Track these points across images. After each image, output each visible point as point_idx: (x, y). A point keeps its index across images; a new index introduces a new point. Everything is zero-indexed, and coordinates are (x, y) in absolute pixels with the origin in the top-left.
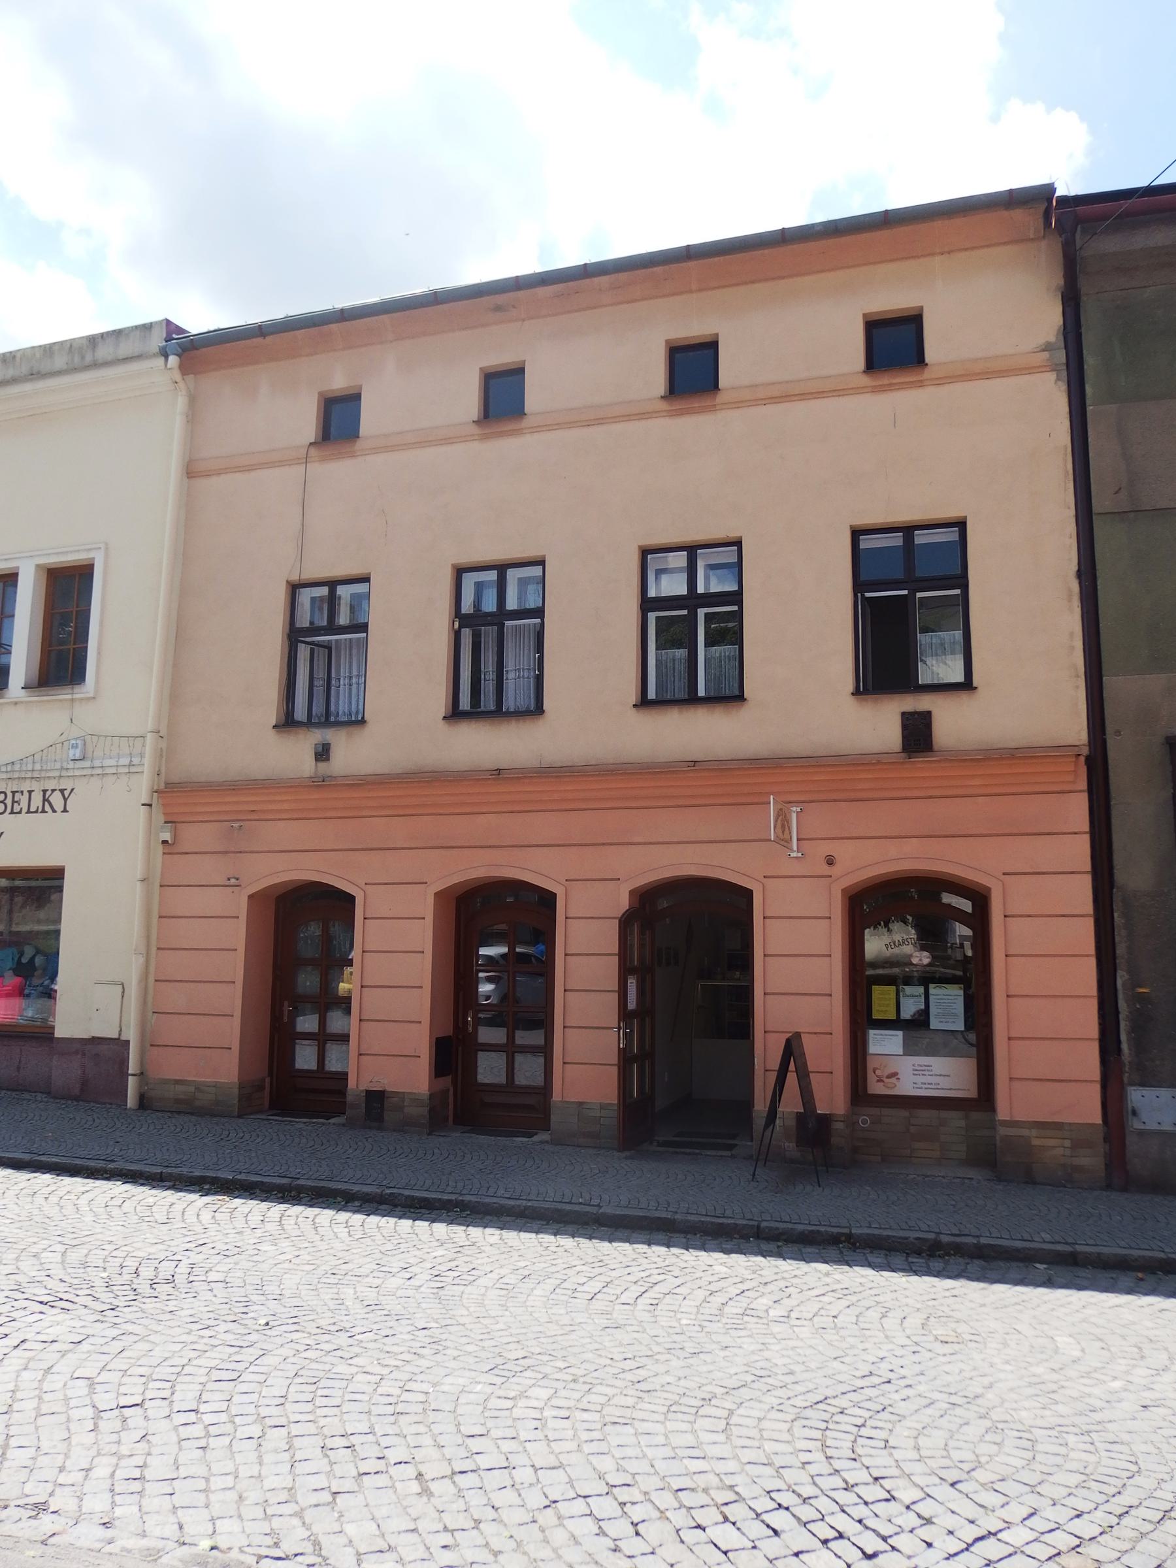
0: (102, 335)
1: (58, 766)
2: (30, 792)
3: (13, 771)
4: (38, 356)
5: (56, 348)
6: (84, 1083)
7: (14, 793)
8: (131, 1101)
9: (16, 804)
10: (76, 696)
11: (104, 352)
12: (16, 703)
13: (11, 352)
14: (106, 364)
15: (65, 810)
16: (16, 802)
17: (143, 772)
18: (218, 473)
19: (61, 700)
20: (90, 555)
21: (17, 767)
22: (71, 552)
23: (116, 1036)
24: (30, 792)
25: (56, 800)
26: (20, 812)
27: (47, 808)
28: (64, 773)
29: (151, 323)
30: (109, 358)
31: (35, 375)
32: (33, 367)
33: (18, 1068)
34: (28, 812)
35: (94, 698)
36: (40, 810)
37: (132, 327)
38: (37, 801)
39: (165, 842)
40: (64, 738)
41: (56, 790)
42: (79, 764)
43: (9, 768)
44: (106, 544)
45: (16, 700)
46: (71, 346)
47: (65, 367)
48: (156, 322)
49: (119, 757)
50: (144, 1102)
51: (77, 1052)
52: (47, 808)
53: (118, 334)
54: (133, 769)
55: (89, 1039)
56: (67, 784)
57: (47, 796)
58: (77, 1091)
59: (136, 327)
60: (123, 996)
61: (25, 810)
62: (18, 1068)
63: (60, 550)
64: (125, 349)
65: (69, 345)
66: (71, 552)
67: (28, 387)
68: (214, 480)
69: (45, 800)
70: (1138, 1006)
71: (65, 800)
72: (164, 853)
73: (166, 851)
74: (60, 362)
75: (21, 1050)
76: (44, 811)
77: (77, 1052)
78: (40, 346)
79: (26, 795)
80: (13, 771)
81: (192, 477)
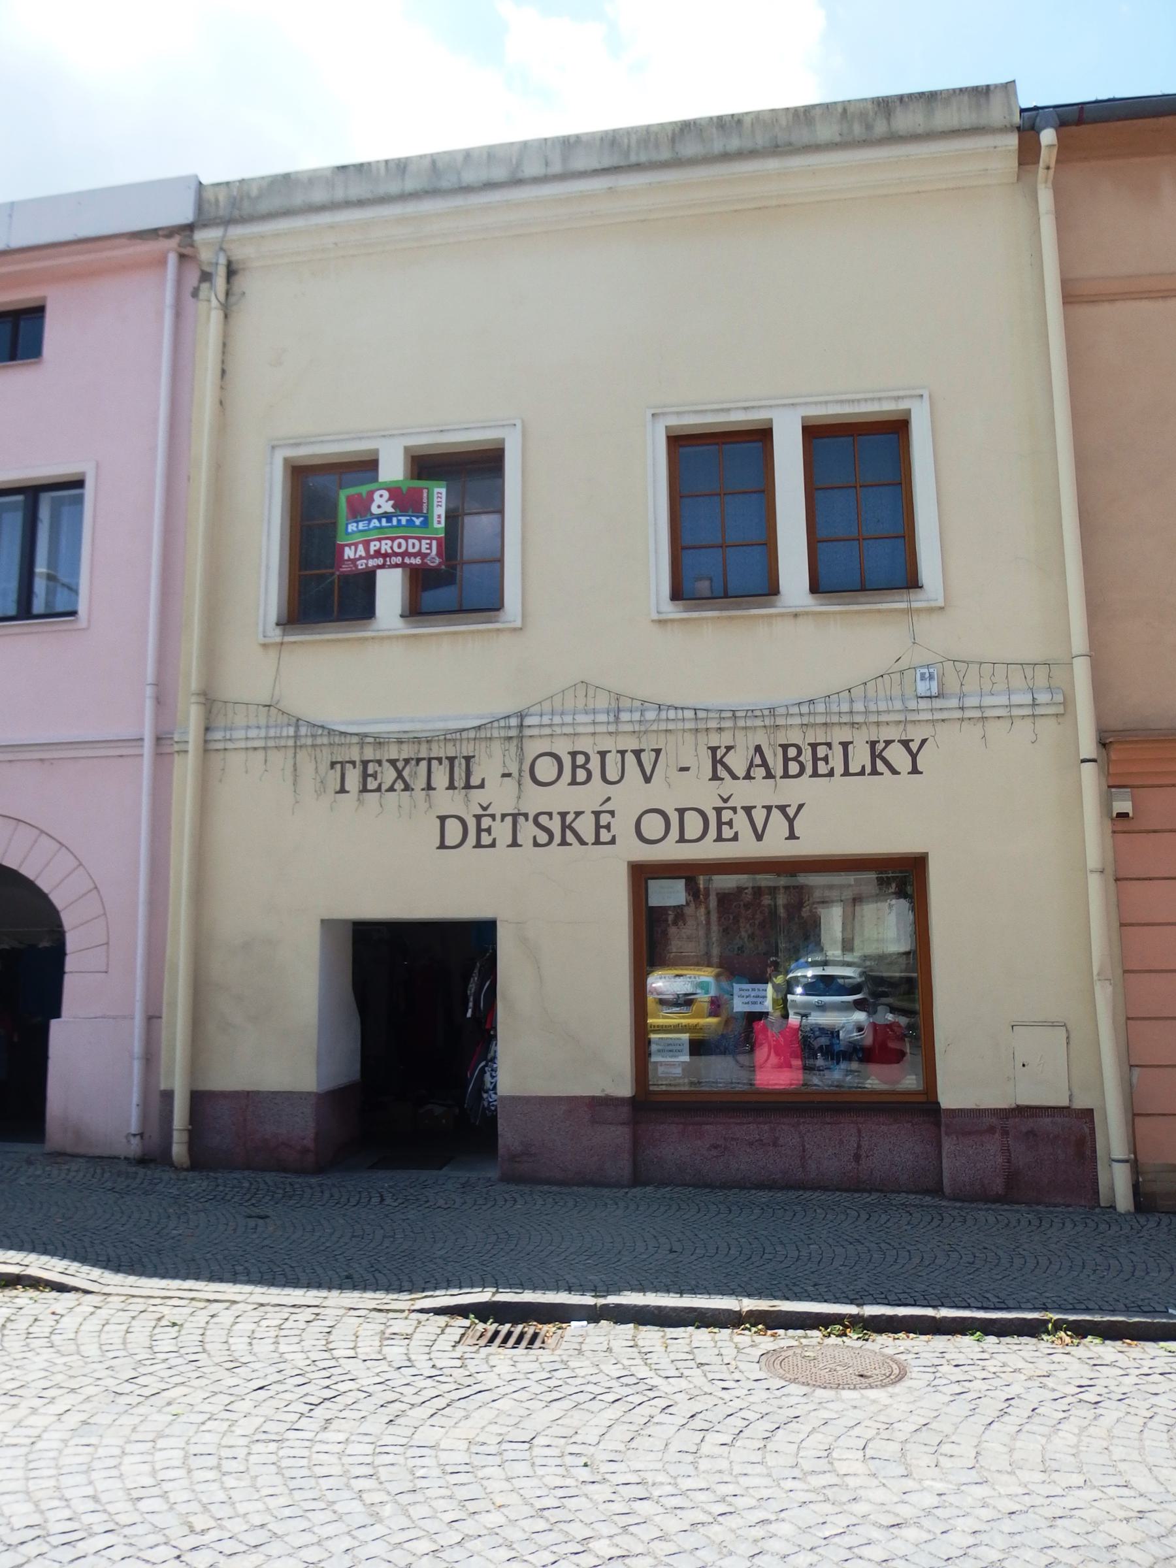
0: (901, 98)
1: (263, 733)
2: (845, 745)
3: (815, 714)
4: (784, 122)
5: (818, 111)
6: (1012, 1177)
7: (814, 746)
8: (1124, 1201)
9: (370, 779)
10: (915, 605)
11: (904, 121)
12: (796, 615)
13: (733, 115)
14: (693, 162)
15: (915, 770)
16: (371, 775)
17: (186, 752)
18: (1112, 298)
19: (879, 611)
20: (903, 405)
21: (820, 708)
22: (866, 400)
23: (1065, 1103)
24: (845, 745)
25: (897, 756)
26: (831, 774)
27: (880, 766)
28: (911, 717)
29: (988, 86)
30: (920, 130)
31: (777, 149)
32: (776, 137)
33: (857, 1158)
34: (846, 773)
35: (521, 629)
36: (868, 770)
37: (954, 90)
38: (860, 757)
39: (1123, 816)
40: (903, 665)
41: (894, 741)
42: (938, 704)
43: (805, 709)
44: (523, 421)
45: (798, 610)
46: (845, 111)
47: (838, 139)
48: (996, 86)
49: (1010, 692)
50: (1144, 1201)
51: (991, 1130)
52: (880, 766)
53: (930, 98)
54: (1039, 710)
55: (1013, 1110)
56: (916, 734)
57: (718, 758)
58: (998, 1186)
59: (962, 91)
60: (1068, 1044)
61: (839, 769)
62: (857, 1158)
63: (844, 397)
64: (944, 118)
65: (840, 110)
66: (866, 400)
67: (772, 164)
68: (1105, 309)
69: (875, 756)
70: (16, 1039)
71: (914, 757)
72: (1114, 832)
73: (1119, 828)
74: (826, 131)
75: (859, 1131)
76: (875, 772)
77: (991, 1130)
78: (788, 109)
79: (838, 750)
80: (563, 724)
81: (1071, 303)
